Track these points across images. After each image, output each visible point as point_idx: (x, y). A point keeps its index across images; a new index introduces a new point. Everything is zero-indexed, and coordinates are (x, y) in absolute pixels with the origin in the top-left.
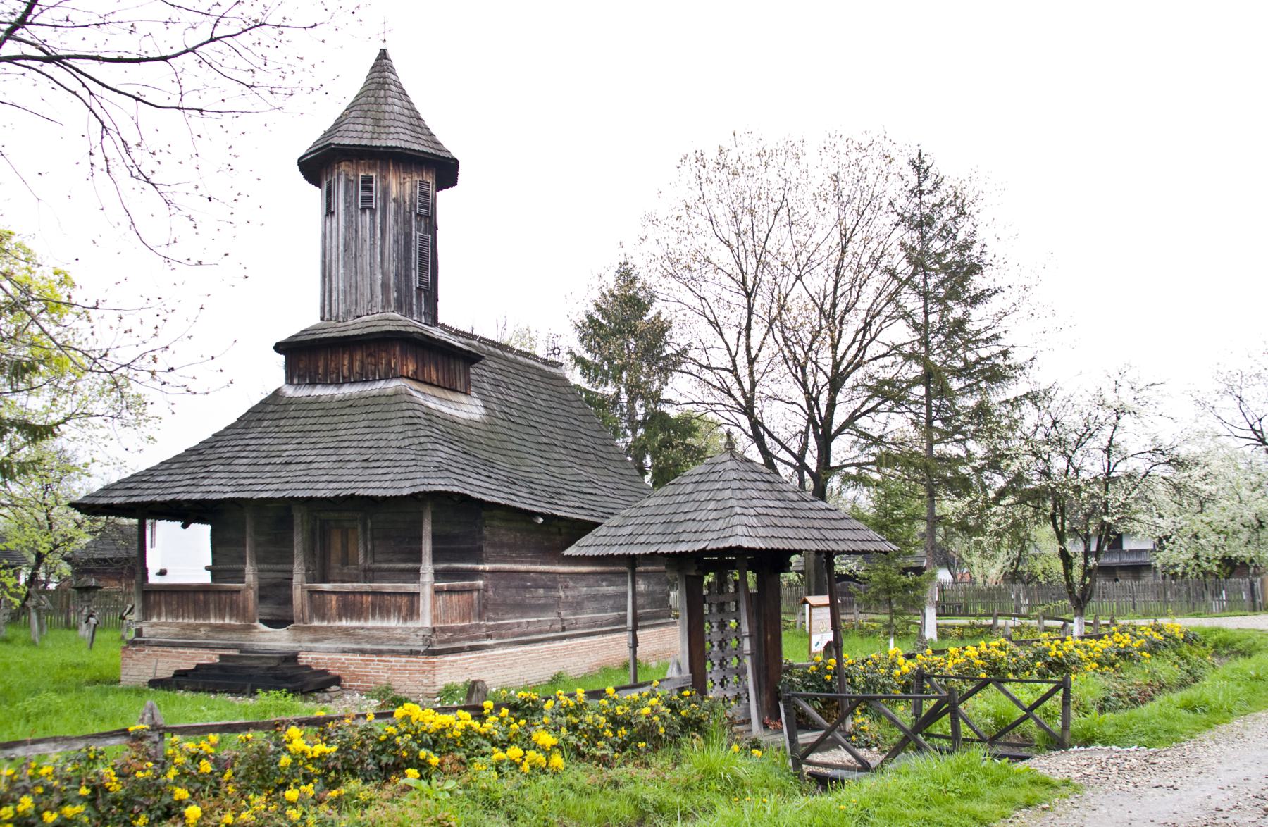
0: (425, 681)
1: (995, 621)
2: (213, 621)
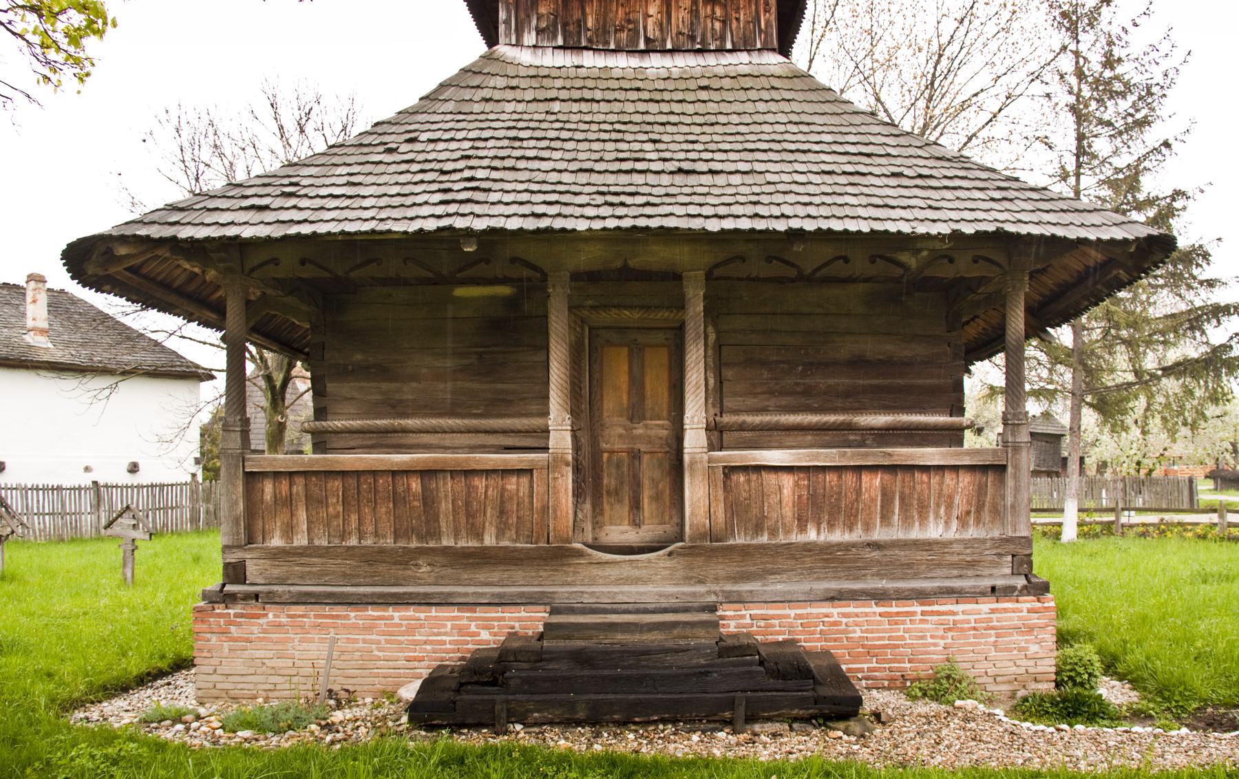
0: (1034, 648)
1: (1118, 518)
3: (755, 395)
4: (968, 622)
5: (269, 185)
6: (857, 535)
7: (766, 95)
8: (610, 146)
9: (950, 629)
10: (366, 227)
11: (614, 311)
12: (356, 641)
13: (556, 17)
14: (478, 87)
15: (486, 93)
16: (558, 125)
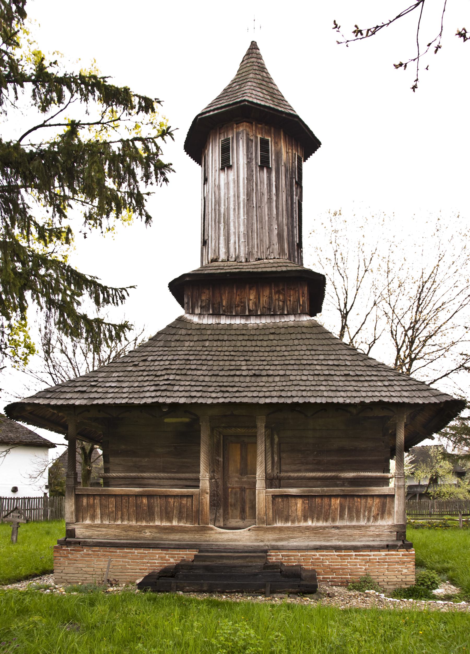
0: (405, 571)
2: (158, 523)
4: (376, 559)
5: (85, 381)
6: (328, 524)
7: (299, 336)
8: (227, 363)
9: (367, 562)
10: (124, 401)
11: (233, 429)
12: (119, 561)
13: (209, 301)
14: (174, 334)
15: (177, 337)
16: (206, 353)
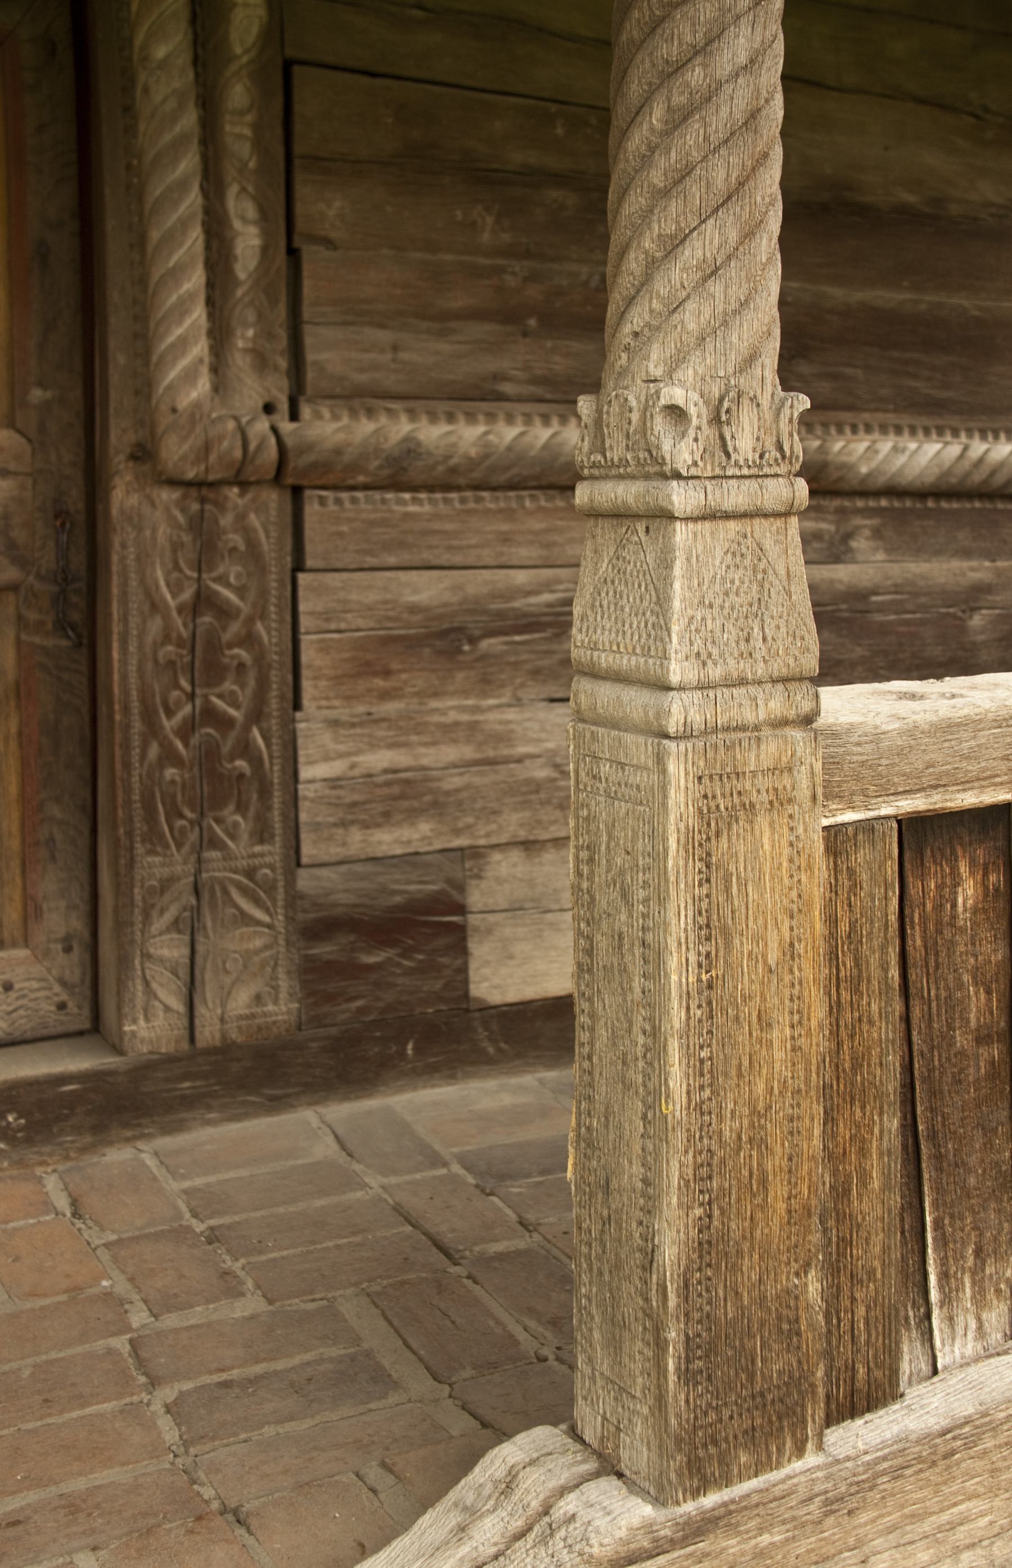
3: (443, 321)
